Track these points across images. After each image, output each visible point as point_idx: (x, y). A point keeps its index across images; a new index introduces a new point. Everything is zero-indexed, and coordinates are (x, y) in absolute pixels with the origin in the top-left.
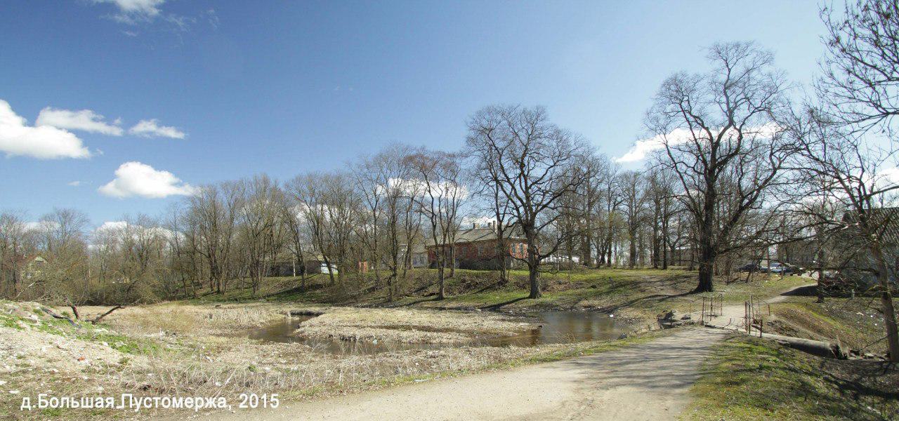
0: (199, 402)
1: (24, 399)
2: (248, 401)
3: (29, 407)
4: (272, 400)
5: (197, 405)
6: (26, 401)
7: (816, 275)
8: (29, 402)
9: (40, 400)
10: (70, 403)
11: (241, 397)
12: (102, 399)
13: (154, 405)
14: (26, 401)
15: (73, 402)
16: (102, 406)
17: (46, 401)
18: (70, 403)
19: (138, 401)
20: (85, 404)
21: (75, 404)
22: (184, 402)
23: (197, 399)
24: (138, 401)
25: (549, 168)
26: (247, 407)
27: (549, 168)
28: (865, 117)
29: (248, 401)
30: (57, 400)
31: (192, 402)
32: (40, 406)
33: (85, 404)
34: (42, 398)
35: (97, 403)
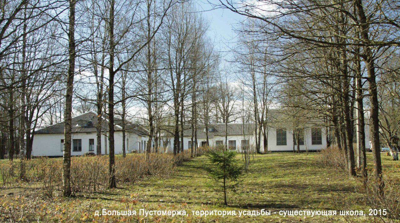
0: (174, 212)
1: (96, 211)
2: (373, 212)
3: (98, 215)
4: (384, 212)
5: (223, 215)
6: (97, 212)
7: (25, 134)
8: (98, 213)
9: (103, 212)
10: (116, 214)
11: (369, 210)
12: (310, 211)
13: (303, 214)
14: (97, 212)
15: (118, 213)
16: (331, 214)
17: (259, 213)
18: (116, 214)
19: (147, 212)
20: (341, 214)
21: (119, 214)
22: (167, 213)
23: (173, 211)
24: (147, 212)
25: (157, 30)
26: (372, 215)
27: (157, 30)
28: (212, 5)
29: (373, 212)
30: (221, 212)
31: (171, 213)
32: (103, 215)
33: (341, 214)
34: (385, 211)
35: (329, 213)
